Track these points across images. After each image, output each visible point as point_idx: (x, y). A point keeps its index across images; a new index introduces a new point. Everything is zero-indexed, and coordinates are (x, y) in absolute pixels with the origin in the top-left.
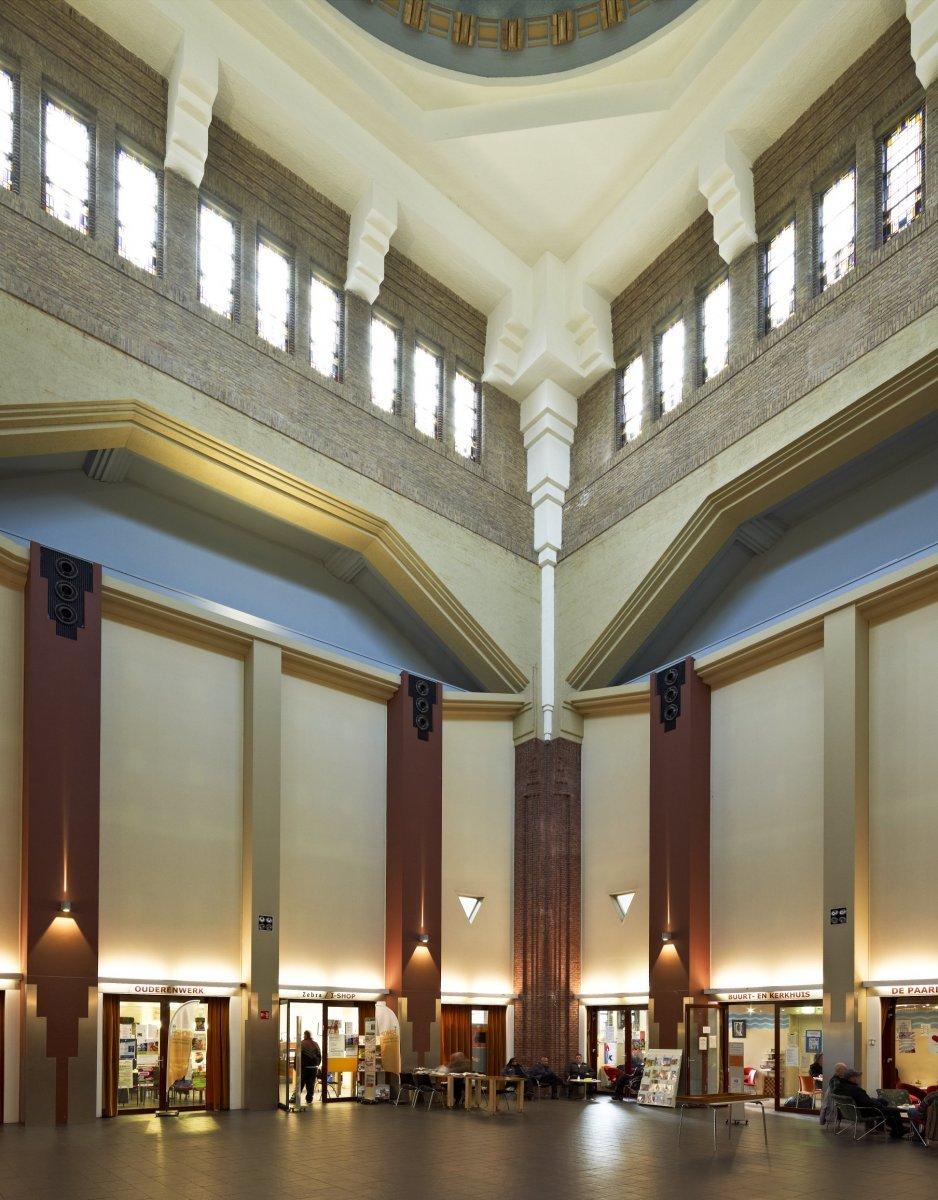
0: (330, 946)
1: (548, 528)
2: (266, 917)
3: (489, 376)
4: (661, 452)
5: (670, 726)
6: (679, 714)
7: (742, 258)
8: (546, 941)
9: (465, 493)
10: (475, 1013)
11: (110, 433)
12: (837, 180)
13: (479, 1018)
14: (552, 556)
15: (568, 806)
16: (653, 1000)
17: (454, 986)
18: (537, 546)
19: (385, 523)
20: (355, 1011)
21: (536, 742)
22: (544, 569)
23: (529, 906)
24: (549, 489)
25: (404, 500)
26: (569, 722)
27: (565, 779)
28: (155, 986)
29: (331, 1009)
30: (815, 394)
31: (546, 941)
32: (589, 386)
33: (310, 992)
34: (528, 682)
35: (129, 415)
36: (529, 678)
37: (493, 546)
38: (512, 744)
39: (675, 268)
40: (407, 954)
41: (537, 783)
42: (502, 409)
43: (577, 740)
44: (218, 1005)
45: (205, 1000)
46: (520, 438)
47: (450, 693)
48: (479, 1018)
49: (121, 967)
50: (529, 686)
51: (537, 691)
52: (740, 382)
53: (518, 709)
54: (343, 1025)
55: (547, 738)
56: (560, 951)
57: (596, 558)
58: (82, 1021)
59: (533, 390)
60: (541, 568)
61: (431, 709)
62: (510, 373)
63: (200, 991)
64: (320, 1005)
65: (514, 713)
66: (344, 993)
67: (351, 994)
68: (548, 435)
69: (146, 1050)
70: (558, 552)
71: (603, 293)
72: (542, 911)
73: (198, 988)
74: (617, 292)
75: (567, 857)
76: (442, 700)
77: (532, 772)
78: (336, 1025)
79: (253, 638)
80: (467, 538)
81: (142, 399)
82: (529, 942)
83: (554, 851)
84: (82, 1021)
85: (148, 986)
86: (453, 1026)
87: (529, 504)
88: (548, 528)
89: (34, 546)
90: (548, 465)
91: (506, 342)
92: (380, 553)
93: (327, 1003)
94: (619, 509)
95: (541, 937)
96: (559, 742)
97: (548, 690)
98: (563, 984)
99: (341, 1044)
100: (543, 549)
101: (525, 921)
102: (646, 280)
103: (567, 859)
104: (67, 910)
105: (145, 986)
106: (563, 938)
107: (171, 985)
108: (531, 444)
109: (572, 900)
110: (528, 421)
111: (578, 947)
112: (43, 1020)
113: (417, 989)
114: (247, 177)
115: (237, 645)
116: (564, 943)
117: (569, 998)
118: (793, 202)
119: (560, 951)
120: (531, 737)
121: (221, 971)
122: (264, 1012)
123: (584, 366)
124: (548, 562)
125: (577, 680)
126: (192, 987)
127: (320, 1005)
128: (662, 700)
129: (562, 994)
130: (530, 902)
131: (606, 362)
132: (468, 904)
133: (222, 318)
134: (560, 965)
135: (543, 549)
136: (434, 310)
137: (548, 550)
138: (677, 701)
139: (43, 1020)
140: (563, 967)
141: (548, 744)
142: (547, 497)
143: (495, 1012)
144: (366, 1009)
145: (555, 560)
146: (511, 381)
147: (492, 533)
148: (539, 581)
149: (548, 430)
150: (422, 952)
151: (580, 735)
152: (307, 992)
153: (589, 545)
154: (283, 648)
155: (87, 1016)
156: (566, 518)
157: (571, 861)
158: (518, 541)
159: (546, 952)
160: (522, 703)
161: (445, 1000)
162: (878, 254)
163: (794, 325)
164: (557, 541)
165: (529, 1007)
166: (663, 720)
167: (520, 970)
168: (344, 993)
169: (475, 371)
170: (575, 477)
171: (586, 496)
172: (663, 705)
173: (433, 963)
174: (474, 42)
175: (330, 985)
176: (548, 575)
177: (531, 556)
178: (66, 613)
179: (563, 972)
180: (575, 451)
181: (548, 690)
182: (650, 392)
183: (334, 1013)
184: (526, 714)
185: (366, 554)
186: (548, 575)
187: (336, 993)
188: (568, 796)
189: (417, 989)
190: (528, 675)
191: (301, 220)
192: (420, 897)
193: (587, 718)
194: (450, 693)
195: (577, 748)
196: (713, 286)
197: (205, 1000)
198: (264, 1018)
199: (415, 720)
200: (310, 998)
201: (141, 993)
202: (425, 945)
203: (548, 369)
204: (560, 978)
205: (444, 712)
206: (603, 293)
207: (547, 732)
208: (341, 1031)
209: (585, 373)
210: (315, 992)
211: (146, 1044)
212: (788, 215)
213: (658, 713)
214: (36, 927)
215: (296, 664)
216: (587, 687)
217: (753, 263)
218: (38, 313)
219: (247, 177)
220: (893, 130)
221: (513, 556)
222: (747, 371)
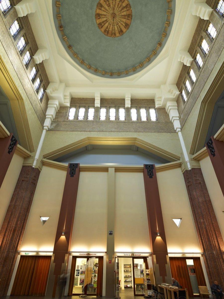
0: (132, 240)
1: (177, 125)
2: (111, 231)
3: (156, 106)
4: (191, 100)
5: (214, 155)
6: (215, 151)
7: (192, 63)
8: (207, 231)
9: (154, 127)
10: (187, 260)
11: (86, 143)
12: (202, 42)
13: (190, 262)
14: (180, 130)
15: (201, 186)
16: (54, 254)
17: (174, 250)
18: (175, 129)
19: (136, 138)
20: (142, 260)
21: (187, 171)
22: (44, 130)
23: (198, 219)
24: (174, 118)
25: (140, 133)
26: (195, 164)
27: (198, 178)
28: (84, 253)
29: (135, 260)
30: (213, 71)
31: (207, 231)
32: (177, 98)
33: (126, 254)
34: (180, 157)
35: (88, 139)
36: (181, 157)
37: (163, 133)
38: (182, 173)
39: (183, 73)
40: (153, 239)
41: (190, 181)
42: (162, 111)
43: (199, 167)
44: (101, 258)
45: (96, 257)
46: (167, 113)
47: (157, 166)
48: (190, 262)
49: (76, 248)
50: (181, 158)
51: (184, 159)
52: (199, 80)
53: (181, 164)
54: (139, 265)
55: (190, 169)
56: (212, 234)
57: (187, 126)
58: (63, 264)
59: (166, 105)
60: (178, 133)
61: (152, 171)
62: (160, 104)
63: (96, 254)
64: (132, 258)
65: (180, 165)
66: (137, 254)
67: (139, 254)
68: (171, 110)
69: (82, 273)
70: (180, 128)
71: (173, 84)
72: (202, 220)
73: (95, 253)
74: (176, 82)
75: (206, 201)
76: (155, 168)
77: (187, 179)
78: (137, 265)
79: (108, 167)
80: (156, 134)
81: (89, 136)
82: (201, 232)
83: (200, 200)
84: (63, 264)
85: (83, 253)
86: (179, 266)
87: (172, 123)
88: (177, 125)
89: (144, 165)
90: (173, 114)
91: (158, 100)
92: (138, 143)
93: (134, 258)
94: (188, 114)
95: (204, 229)
96: (193, 169)
97: (186, 157)
98: (218, 248)
99: (139, 273)
100: (176, 129)
101: (198, 224)
102: (179, 78)
103: (206, 201)
104: (159, 235)
105: (82, 253)
106: (212, 229)
107: (88, 253)
108: (169, 113)
109: (211, 215)
110: (167, 109)
111: (220, 232)
112: (55, 264)
113: (160, 251)
114: (107, 103)
115: (106, 169)
116: (213, 231)
117: (16, 252)
118: (196, 51)
119: (212, 234)
120: (185, 170)
121: (100, 249)
122: (110, 261)
123: (174, 96)
124: (178, 131)
125: (192, 152)
126: (93, 253)
127: (132, 258)
128: (210, 149)
129: (219, 252)
130: (17, 217)
131: (178, 93)
132: (177, 222)
133: (114, 121)
134: (214, 240)
135: (176, 129)
136: (149, 103)
137: (178, 129)
138: (213, 148)
139: (55, 264)
140: (215, 240)
141: (190, 170)
142: (174, 120)
143: (196, 260)
144: (145, 259)
145: (180, 130)
146: (161, 105)
147: (162, 131)
148: (178, 136)
149: (170, 109)
150: (159, 238)
151: (199, 165)
152: (125, 254)
153: (185, 124)
154: (115, 167)
155: (64, 263)
156: (180, 121)
157: (207, 202)
158: (171, 130)
159: (208, 235)
160: (181, 163)
161: (170, 255)
162: (213, 44)
163: (204, 65)
164: (179, 126)
165: (208, 257)
166: (212, 154)
167: (201, 242)
168: (137, 254)
169: (154, 107)
170: (179, 113)
171: (182, 116)
172: (211, 150)
173: (66, 242)
174: (136, 69)
175: (133, 252)
176: (180, 134)
177: (175, 132)
178: (72, 173)
179: (216, 242)
180: (178, 109)
181: (37, 156)
182: (186, 92)
183: (137, 261)
184: (182, 165)
185: (136, 145)
186: (180, 134)
187: (135, 254)
188: (200, 183)
189: (160, 251)
190: (179, 155)
191: (117, 103)
192: (65, 219)
193: (200, 161)
194: (157, 166)
195: (200, 170)
196: (190, 71)
197: (96, 257)
198: (110, 263)
199: (150, 173)
200: (126, 256)
201: (81, 255)
202: (159, 236)
203: (167, 100)
204: (215, 245)
205: (156, 171)
206: (173, 84)
207: (189, 167)
208: (139, 268)
209: (175, 97)
210: (128, 254)
211: (82, 271)
212: (197, 52)
213: (210, 153)
214: (153, 239)
215: (117, 170)
216: (196, 153)
217: (194, 63)
218: (74, 132)
219: (107, 103)
220: (207, 28)
221: (169, 133)
222: (199, 78)
